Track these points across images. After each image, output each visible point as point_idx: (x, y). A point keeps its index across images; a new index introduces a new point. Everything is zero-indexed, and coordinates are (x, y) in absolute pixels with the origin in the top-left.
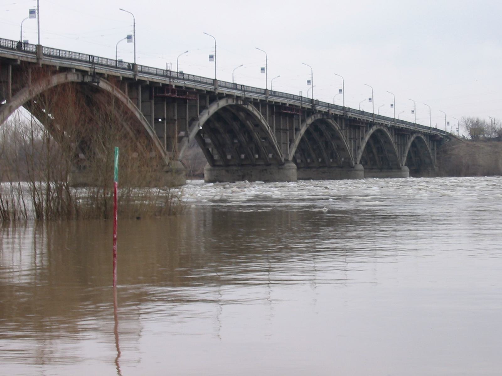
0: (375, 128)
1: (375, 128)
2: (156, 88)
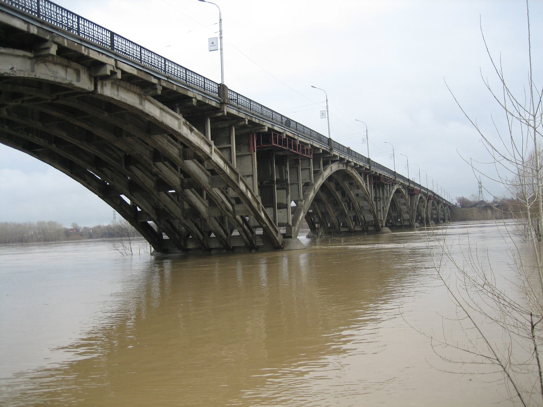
0: (334, 167)
1: (334, 167)
2: (258, 135)
